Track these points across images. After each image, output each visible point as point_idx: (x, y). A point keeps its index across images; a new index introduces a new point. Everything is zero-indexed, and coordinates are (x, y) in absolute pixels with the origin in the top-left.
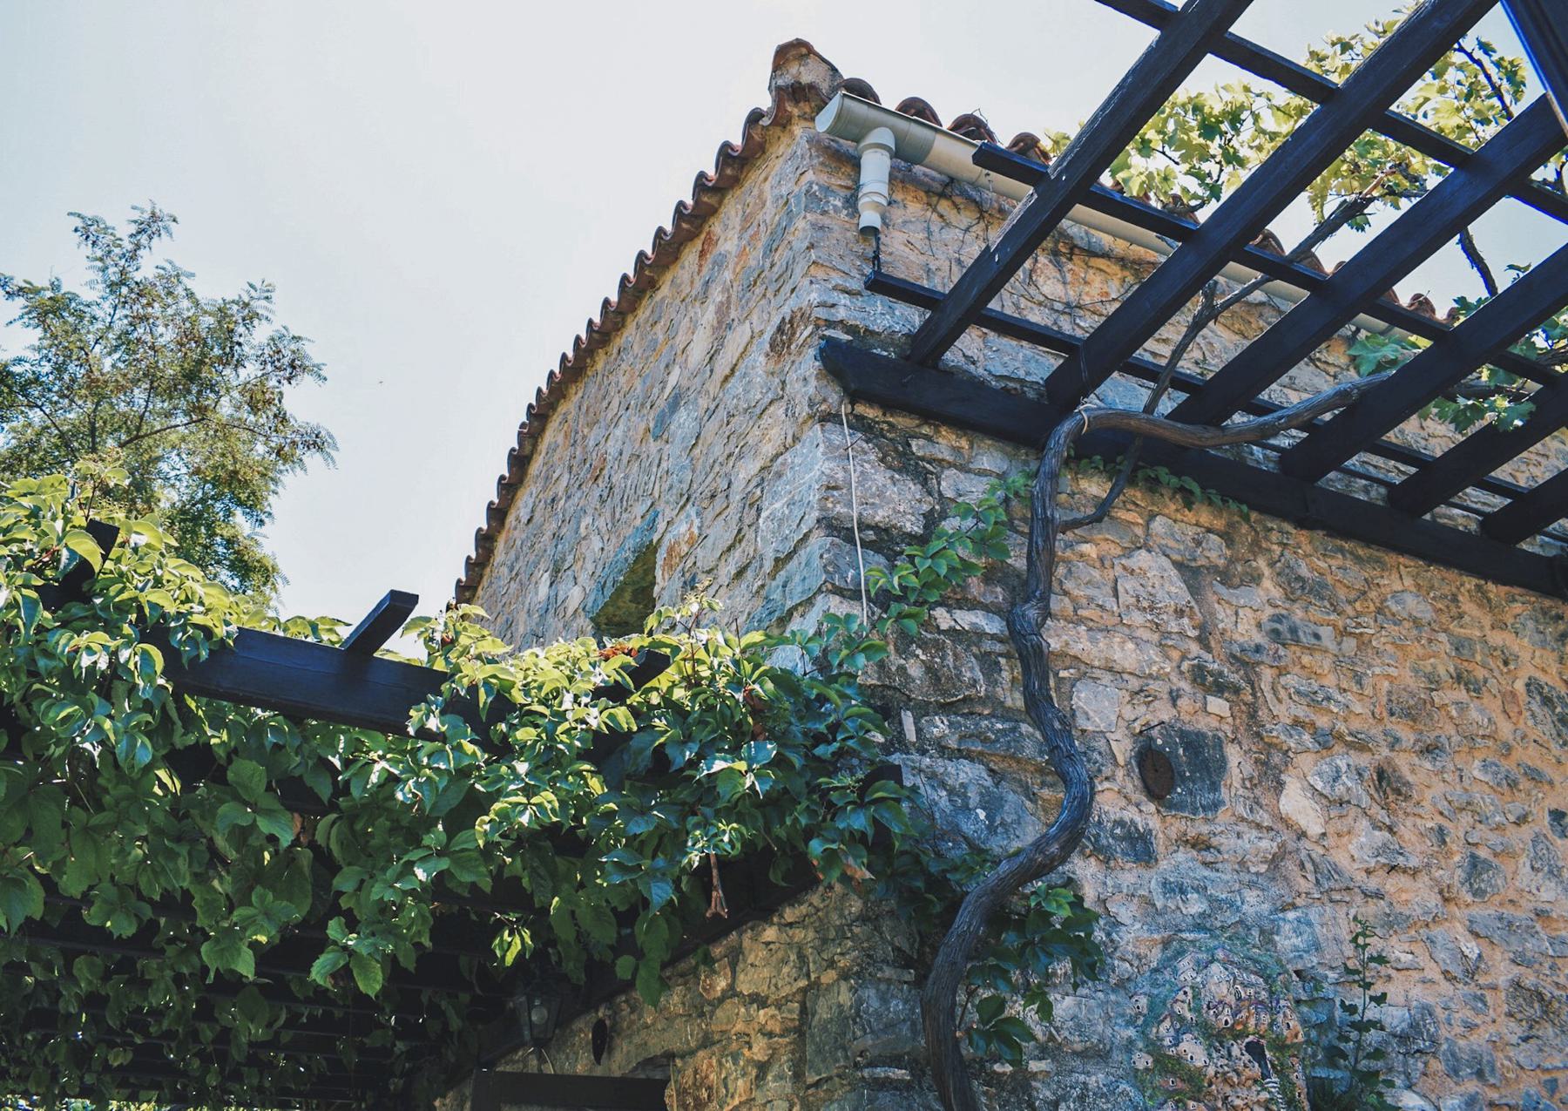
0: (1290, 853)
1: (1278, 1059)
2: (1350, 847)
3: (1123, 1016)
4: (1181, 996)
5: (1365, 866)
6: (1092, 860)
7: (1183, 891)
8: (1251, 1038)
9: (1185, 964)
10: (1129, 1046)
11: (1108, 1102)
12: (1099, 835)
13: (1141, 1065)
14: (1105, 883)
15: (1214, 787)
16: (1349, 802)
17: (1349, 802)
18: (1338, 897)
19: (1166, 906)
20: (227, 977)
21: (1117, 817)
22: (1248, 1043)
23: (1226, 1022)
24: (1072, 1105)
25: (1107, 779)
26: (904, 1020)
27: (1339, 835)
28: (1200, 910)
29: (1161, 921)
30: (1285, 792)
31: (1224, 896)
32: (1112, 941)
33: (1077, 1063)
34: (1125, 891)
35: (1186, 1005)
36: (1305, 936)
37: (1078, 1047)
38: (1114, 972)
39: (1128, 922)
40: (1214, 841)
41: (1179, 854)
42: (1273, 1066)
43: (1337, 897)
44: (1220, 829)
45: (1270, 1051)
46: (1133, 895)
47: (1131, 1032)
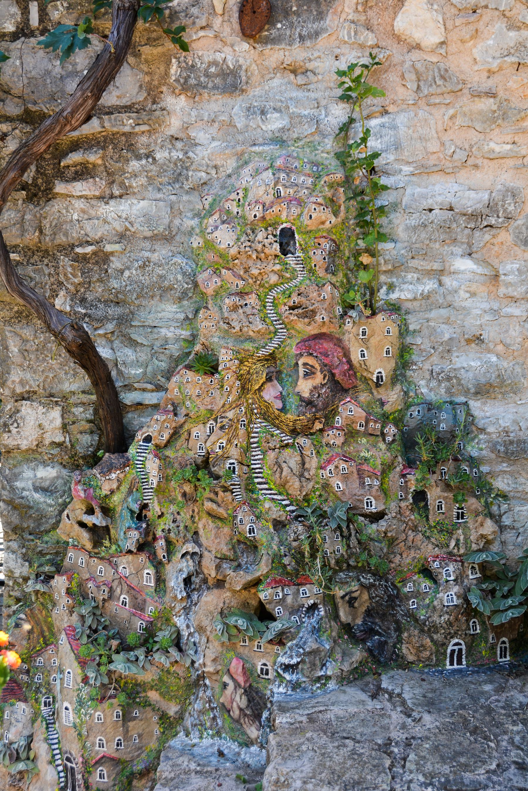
0: (395, 65)
1: (304, 240)
2: (474, 51)
3: (192, 210)
4: (233, 196)
5: (487, 67)
6: (183, 97)
7: (263, 113)
8: (284, 225)
9: (246, 171)
10: (190, 233)
11: (164, 269)
12: (189, 77)
13: (195, 245)
14: (190, 114)
15: (321, 16)
16: (486, 7)
17: (486, 7)
18: (437, 101)
19: (247, 126)
20: (13, 700)
21: (211, 59)
22: (282, 230)
23: (255, 216)
24: (134, 272)
25: (202, 28)
26: (14, 224)
27: (463, 41)
28: (281, 126)
29: (240, 138)
30: (404, 9)
31: (306, 113)
32: (188, 158)
33: (147, 244)
34: (206, 119)
35: (235, 203)
36: (386, 139)
37: (149, 234)
38: (187, 180)
39: (205, 142)
40: (310, 66)
41: (275, 80)
42: (301, 245)
43: (433, 100)
44: (316, 54)
45: (299, 234)
46: (213, 121)
47: (194, 222)
